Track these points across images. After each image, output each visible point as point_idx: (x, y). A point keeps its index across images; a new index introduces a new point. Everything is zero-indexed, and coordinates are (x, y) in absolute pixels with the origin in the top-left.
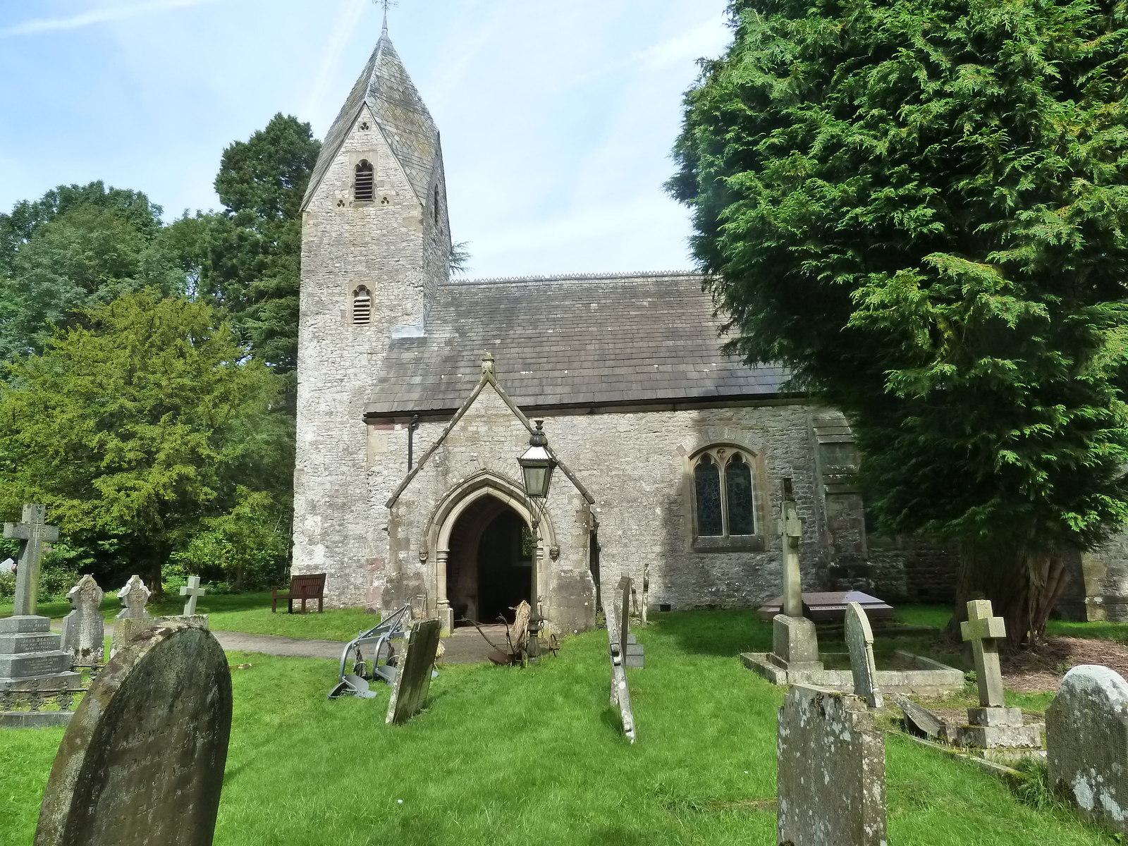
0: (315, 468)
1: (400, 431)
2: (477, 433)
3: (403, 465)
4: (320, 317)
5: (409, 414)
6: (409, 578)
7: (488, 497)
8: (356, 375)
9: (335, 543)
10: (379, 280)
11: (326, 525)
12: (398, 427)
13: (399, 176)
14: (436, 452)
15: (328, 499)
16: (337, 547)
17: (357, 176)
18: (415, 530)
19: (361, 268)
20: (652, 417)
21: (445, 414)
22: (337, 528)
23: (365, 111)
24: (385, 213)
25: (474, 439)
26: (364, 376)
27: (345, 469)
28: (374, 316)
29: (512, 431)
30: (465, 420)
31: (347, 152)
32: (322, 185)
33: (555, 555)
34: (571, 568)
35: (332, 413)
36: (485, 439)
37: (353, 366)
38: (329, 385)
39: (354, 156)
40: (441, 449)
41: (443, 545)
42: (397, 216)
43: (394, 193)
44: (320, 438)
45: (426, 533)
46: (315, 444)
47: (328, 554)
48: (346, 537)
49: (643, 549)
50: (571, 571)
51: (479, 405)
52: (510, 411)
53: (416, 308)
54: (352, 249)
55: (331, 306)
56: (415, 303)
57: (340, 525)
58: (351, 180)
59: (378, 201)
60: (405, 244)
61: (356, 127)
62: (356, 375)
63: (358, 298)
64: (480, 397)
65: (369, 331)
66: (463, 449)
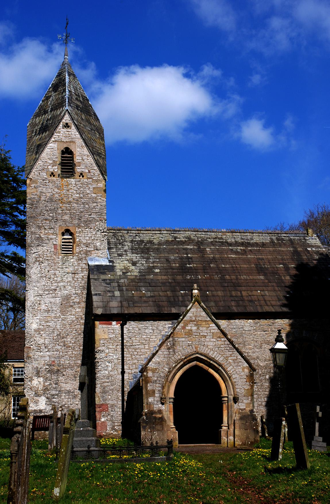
0: (39, 346)
1: (115, 325)
2: (191, 330)
3: (118, 347)
4: (40, 248)
7: (196, 366)
8: (65, 287)
9: (53, 395)
10: (79, 226)
11: (47, 384)
12: (114, 323)
14: (168, 340)
15: (47, 367)
16: (54, 398)
17: (62, 157)
19: (66, 217)
20: (263, 322)
21: (174, 317)
24: (81, 184)
25: (190, 333)
26: (70, 288)
29: (210, 330)
30: (184, 323)
31: (56, 141)
33: (236, 400)
34: (245, 407)
35: (49, 310)
36: (196, 334)
37: (62, 281)
38: (47, 292)
39: (62, 144)
40: (171, 339)
41: (172, 394)
42: (90, 186)
43: (87, 171)
44: (41, 327)
46: (38, 331)
47: (48, 403)
49: (260, 400)
50: (245, 409)
51: (191, 315)
52: (209, 319)
53: (102, 246)
54: (61, 205)
55: (48, 241)
57: (56, 384)
59: (77, 175)
60: (95, 204)
62: (65, 287)
63: (65, 237)
64: (192, 310)
65: (73, 260)
66: (184, 339)
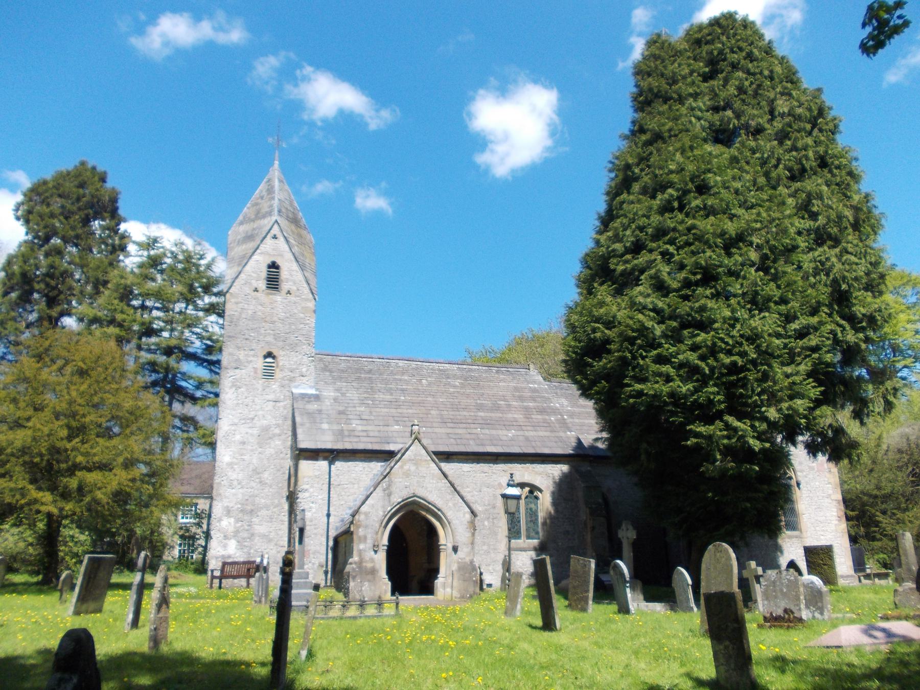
2: (409, 470)
4: (237, 371)
5: (331, 451)
6: (366, 562)
13: (299, 276)
18: (370, 531)
22: (247, 528)
23: (276, 226)
25: (407, 474)
27: (253, 484)
28: (278, 374)
32: (242, 275)
40: (387, 479)
44: (235, 460)
45: (377, 533)
46: (231, 465)
48: (253, 535)
56: (308, 367)
58: (264, 274)
60: (302, 326)
61: (269, 236)
